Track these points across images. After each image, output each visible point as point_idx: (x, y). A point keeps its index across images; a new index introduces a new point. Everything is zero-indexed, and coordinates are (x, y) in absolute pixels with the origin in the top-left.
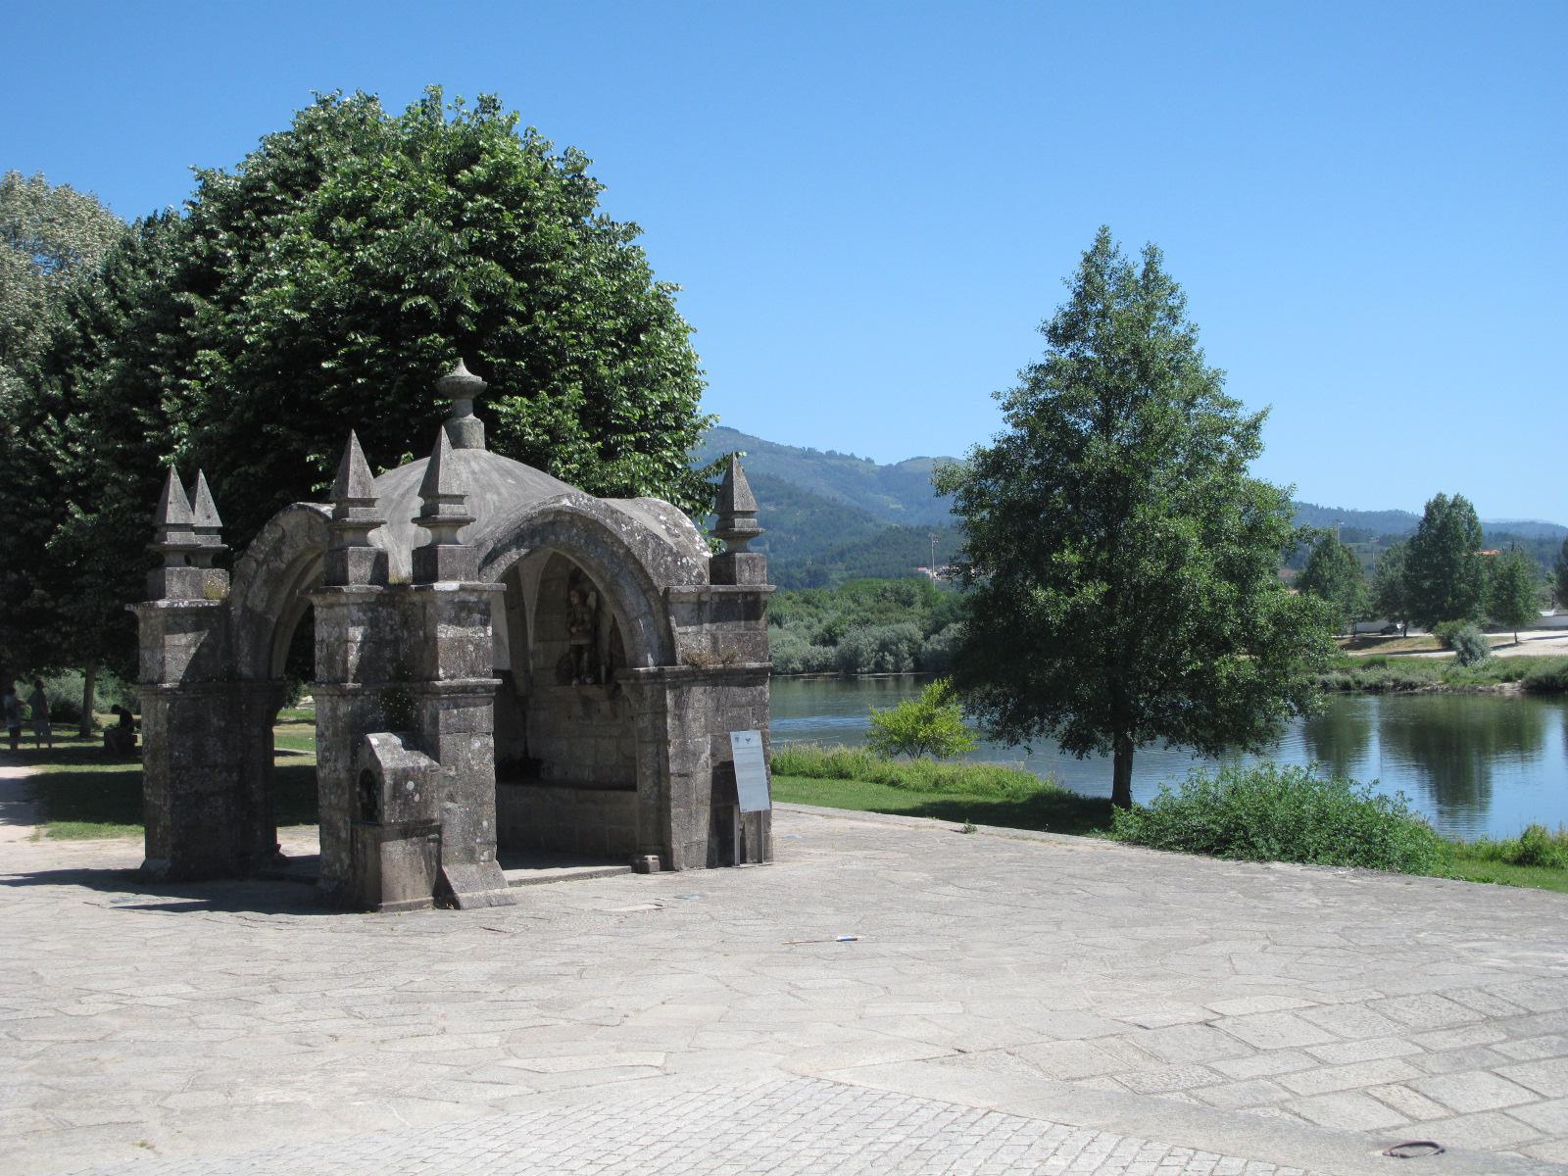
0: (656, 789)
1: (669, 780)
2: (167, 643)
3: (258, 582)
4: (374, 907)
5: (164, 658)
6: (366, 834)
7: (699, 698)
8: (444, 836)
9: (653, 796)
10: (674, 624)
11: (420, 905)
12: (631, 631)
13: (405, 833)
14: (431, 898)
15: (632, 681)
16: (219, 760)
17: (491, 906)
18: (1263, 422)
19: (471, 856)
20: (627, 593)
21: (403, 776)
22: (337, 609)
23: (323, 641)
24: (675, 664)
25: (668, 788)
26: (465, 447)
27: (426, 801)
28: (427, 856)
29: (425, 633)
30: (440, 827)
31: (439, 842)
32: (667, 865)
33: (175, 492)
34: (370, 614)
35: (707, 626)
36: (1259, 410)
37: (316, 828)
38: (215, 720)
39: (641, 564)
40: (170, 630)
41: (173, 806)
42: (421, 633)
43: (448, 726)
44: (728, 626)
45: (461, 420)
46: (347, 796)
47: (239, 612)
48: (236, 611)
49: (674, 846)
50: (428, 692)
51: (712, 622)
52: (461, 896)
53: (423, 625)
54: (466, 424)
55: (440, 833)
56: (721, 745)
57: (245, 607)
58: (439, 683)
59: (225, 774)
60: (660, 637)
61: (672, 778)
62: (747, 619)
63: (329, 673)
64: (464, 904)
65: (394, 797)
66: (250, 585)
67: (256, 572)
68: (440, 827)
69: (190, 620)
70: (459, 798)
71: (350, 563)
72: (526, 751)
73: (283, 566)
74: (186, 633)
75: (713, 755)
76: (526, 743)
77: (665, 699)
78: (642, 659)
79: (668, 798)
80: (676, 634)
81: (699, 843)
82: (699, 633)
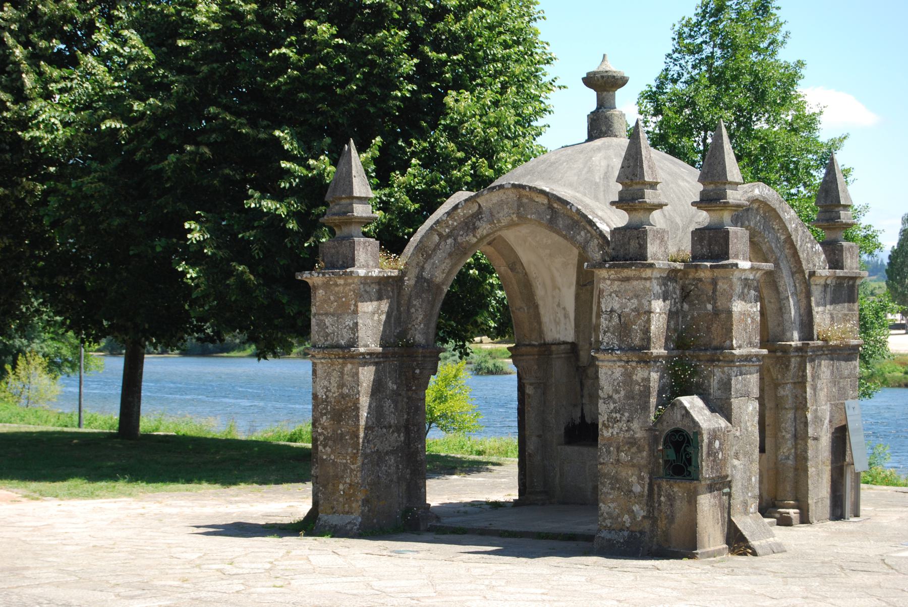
0: (793, 451)
1: (806, 443)
2: (359, 309)
3: (440, 254)
4: (692, 556)
5: (356, 324)
6: (678, 488)
7: (825, 368)
8: (733, 489)
9: (791, 457)
10: (813, 304)
11: (719, 553)
12: (781, 309)
13: (711, 488)
14: (725, 546)
15: (779, 354)
16: (392, 422)
17: (774, 552)
18: (845, 142)
19: (746, 512)
20: (784, 275)
21: (715, 435)
22: (635, 283)
23: (612, 311)
24: (812, 339)
25: (805, 451)
26: (616, 136)
27: (725, 458)
28: (722, 506)
29: (714, 307)
30: (730, 482)
31: (729, 495)
32: (805, 519)
33: (356, 166)
34: (663, 288)
35: (828, 307)
36: (837, 135)
37: (309, 487)
38: (390, 384)
39: (796, 249)
40: (362, 297)
41: (363, 464)
42: (709, 307)
43: (737, 391)
44: (839, 307)
45: (612, 111)
46: (645, 454)
47: (412, 282)
48: (409, 281)
49: (810, 501)
50: (719, 360)
51: (831, 304)
52: (754, 543)
53: (713, 299)
54: (616, 115)
55: (730, 487)
56: (839, 408)
57: (420, 278)
58: (737, 352)
59: (396, 435)
60: (800, 315)
61: (809, 441)
62: (849, 302)
63: (621, 340)
64: (759, 551)
65: (709, 455)
66: (429, 257)
67: (438, 245)
68: (730, 482)
69: (374, 288)
70: (741, 456)
71: (648, 240)
72: (583, 417)
73: (475, 240)
74: (371, 301)
75: (830, 421)
76: (582, 410)
77: (804, 370)
78: (788, 334)
79: (806, 459)
80: (814, 313)
81: (822, 499)
82: (824, 312)
